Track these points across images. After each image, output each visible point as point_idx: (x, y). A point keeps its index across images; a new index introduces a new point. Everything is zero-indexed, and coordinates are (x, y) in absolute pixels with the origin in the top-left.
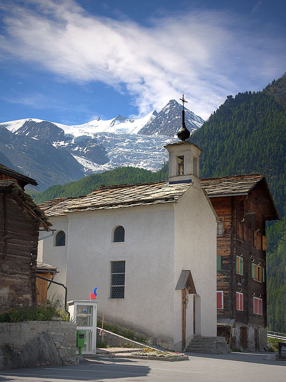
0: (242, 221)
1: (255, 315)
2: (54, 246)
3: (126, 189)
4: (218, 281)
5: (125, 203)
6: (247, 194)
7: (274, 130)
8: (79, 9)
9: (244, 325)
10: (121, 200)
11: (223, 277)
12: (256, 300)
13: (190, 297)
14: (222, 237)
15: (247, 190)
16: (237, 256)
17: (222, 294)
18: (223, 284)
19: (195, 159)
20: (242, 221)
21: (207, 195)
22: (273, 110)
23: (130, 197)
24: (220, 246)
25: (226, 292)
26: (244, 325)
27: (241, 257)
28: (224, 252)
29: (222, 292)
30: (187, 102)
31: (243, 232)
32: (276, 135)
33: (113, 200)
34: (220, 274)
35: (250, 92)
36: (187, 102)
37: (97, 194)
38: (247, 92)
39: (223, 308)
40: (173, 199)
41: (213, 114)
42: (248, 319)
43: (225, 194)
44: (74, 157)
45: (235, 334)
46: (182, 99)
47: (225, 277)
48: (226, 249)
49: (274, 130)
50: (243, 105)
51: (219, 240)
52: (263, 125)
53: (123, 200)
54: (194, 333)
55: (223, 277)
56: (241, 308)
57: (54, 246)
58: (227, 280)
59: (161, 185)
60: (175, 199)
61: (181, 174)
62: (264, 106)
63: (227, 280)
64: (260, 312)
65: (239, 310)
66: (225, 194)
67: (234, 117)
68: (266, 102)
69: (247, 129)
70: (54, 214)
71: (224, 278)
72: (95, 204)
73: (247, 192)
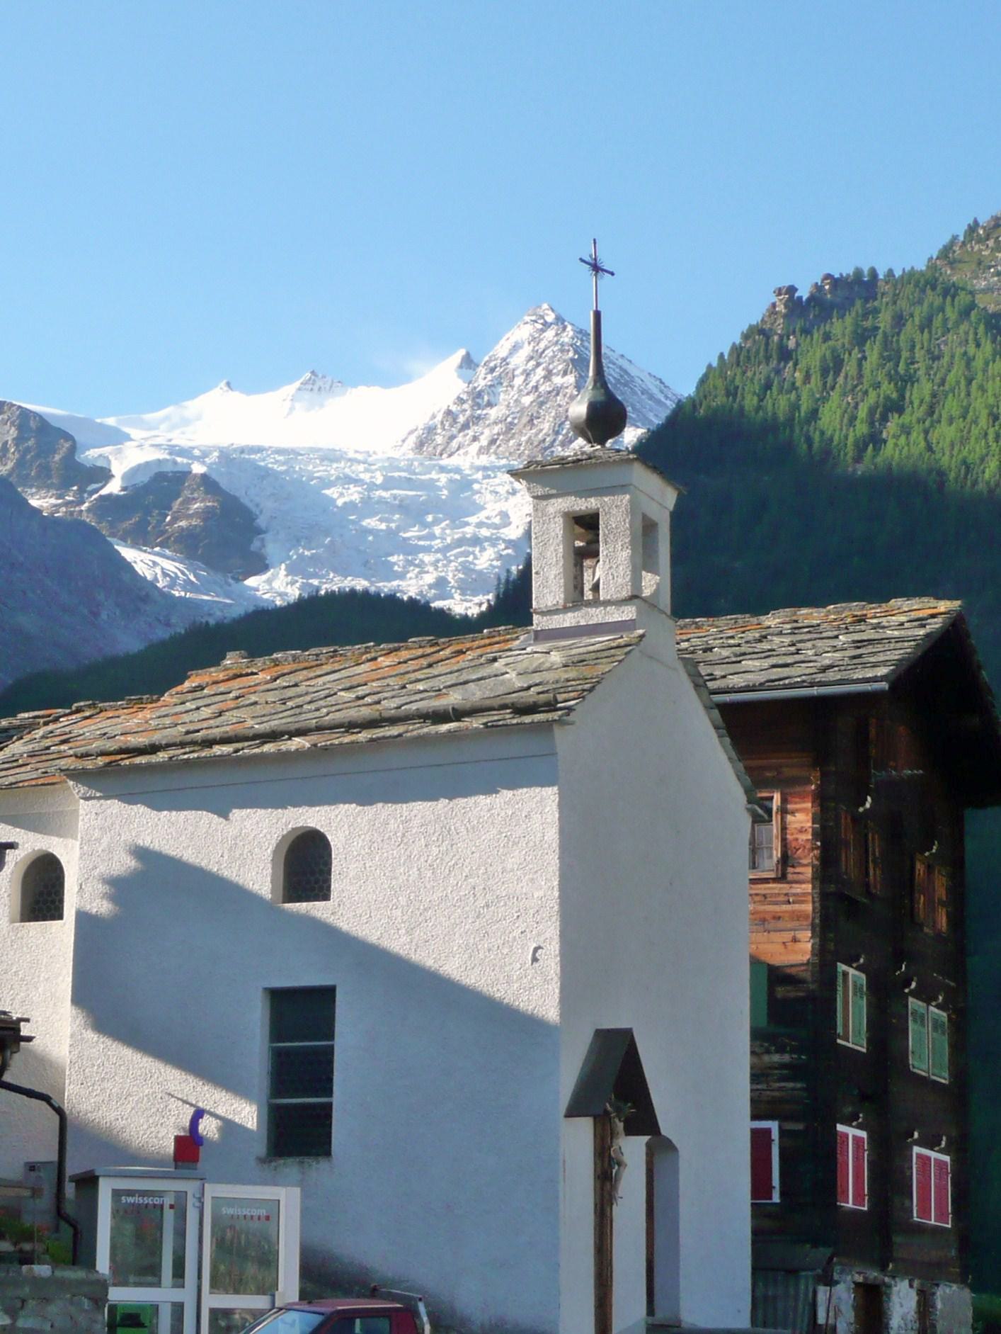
0: (861, 810)
1: (921, 1229)
2: (12, 921)
3: (337, 667)
4: (756, 1077)
5: (332, 727)
6: (884, 685)
7: (975, 431)
8: (275, 464)
9: (873, 1274)
10: (317, 714)
11: (776, 1058)
12: (924, 1161)
13: (633, 1149)
14: (775, 880)
15: (882, 671)
16: (842, 967)
17: (775, 1135)
18: (780, 1089)
19: (648, 528)
20: (861, 810)
21: (705, 693)
22: (971, 349)
23: (359, 698)
24: (764, 920)
25: (791, 1126)
26: (873, 1274)
27: (856, 969)
28: (780, 948)
29: (773, 1126)
30: (612, 274)
31: (867, 857)
32: (984, 451)
33: (281, 715)
34: (766, 1044)
35: (873, 273)
36: (612, 274)
37: (205, 691)
38: (858, 273)
39: (776, 1198)
40: (551, 706)
41: (715, 364)
42: (887, 1244)
43: (786, 687)
44: (128, 553)
45: (831, 1314)
46: (591, 261)
47: (786, 1058)
48: (790, 934)
49: (975, 431)
50: (841, 328)
51: (757, 895)
52: (931, 412)
53: (328, 714)
54: (651, 1311)
55: (776, 1058)
56: (858, 1198)
57: (12, 921)
58: (793, 1071)
59: (496, 647)
60: (559, 705)
61: (588, 595)
62: (934, 329)
63: (793, 1071)
64: (941, 1216)
65: (933, 1222)
66: (786, 687)
67: (807, 378)
68: (943, 312)
69: (862, 428)
70: (11, 779)
71: (783, 1066)
72: (198, 731)
73: (883, 678)
